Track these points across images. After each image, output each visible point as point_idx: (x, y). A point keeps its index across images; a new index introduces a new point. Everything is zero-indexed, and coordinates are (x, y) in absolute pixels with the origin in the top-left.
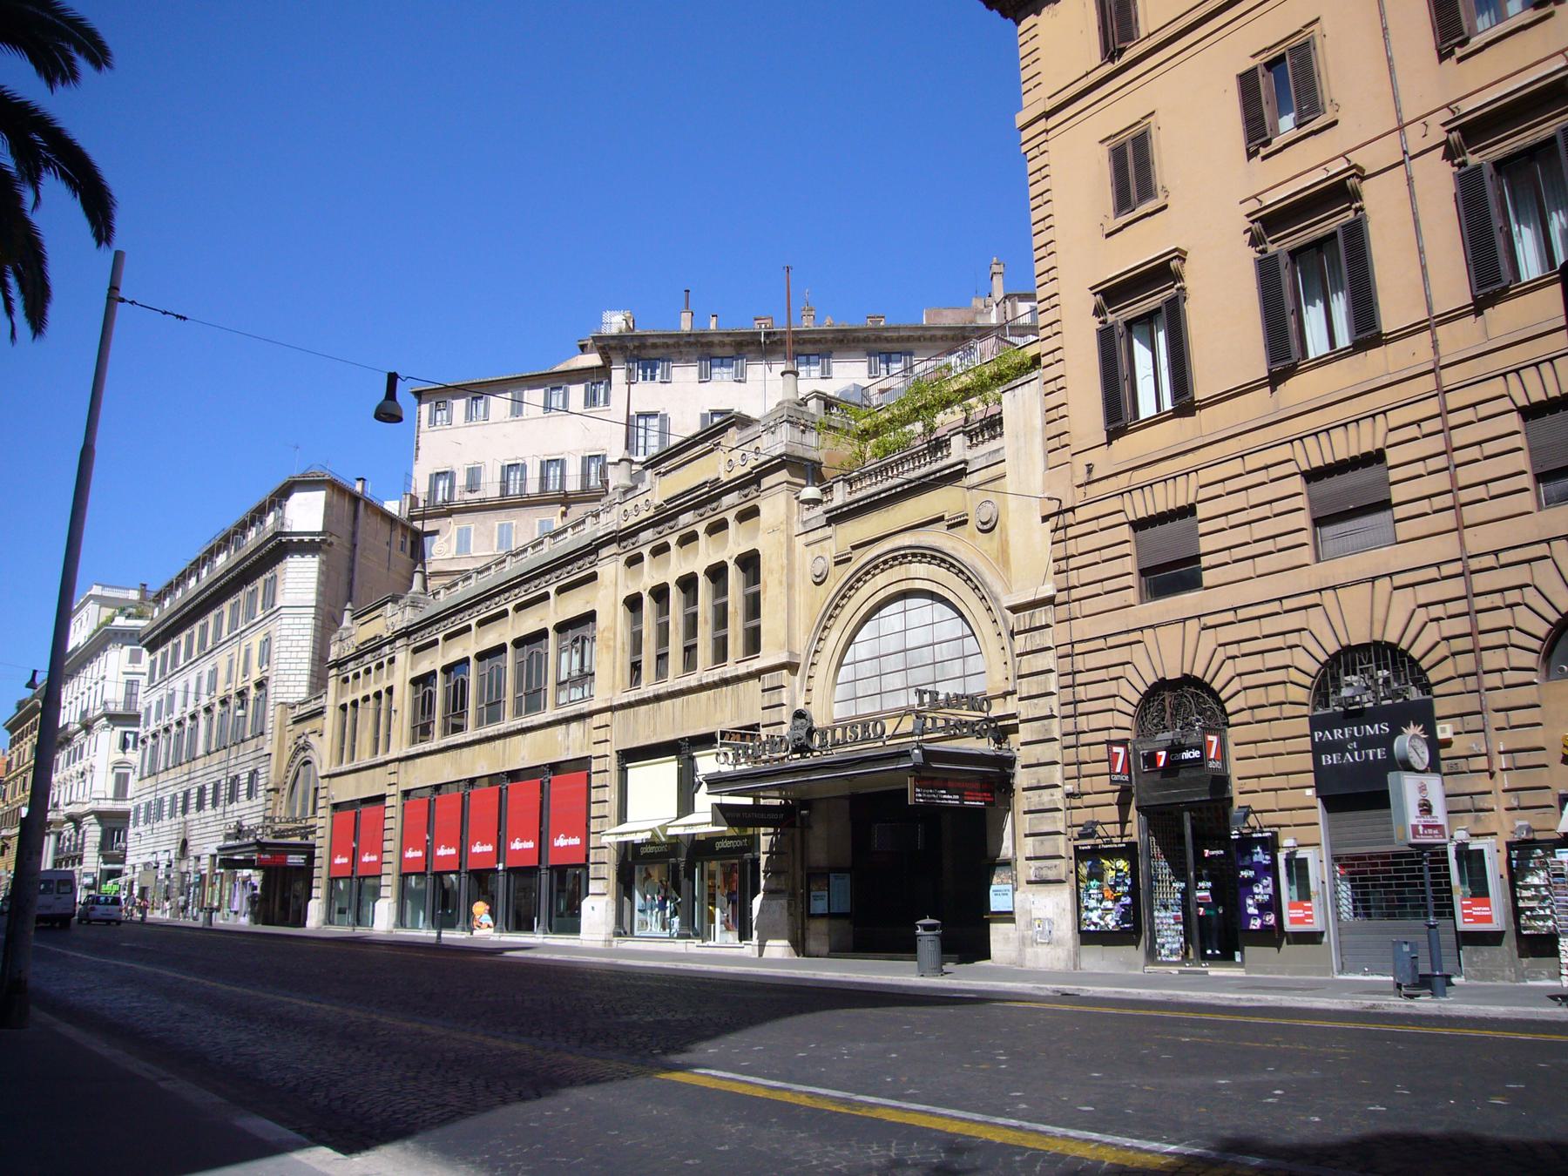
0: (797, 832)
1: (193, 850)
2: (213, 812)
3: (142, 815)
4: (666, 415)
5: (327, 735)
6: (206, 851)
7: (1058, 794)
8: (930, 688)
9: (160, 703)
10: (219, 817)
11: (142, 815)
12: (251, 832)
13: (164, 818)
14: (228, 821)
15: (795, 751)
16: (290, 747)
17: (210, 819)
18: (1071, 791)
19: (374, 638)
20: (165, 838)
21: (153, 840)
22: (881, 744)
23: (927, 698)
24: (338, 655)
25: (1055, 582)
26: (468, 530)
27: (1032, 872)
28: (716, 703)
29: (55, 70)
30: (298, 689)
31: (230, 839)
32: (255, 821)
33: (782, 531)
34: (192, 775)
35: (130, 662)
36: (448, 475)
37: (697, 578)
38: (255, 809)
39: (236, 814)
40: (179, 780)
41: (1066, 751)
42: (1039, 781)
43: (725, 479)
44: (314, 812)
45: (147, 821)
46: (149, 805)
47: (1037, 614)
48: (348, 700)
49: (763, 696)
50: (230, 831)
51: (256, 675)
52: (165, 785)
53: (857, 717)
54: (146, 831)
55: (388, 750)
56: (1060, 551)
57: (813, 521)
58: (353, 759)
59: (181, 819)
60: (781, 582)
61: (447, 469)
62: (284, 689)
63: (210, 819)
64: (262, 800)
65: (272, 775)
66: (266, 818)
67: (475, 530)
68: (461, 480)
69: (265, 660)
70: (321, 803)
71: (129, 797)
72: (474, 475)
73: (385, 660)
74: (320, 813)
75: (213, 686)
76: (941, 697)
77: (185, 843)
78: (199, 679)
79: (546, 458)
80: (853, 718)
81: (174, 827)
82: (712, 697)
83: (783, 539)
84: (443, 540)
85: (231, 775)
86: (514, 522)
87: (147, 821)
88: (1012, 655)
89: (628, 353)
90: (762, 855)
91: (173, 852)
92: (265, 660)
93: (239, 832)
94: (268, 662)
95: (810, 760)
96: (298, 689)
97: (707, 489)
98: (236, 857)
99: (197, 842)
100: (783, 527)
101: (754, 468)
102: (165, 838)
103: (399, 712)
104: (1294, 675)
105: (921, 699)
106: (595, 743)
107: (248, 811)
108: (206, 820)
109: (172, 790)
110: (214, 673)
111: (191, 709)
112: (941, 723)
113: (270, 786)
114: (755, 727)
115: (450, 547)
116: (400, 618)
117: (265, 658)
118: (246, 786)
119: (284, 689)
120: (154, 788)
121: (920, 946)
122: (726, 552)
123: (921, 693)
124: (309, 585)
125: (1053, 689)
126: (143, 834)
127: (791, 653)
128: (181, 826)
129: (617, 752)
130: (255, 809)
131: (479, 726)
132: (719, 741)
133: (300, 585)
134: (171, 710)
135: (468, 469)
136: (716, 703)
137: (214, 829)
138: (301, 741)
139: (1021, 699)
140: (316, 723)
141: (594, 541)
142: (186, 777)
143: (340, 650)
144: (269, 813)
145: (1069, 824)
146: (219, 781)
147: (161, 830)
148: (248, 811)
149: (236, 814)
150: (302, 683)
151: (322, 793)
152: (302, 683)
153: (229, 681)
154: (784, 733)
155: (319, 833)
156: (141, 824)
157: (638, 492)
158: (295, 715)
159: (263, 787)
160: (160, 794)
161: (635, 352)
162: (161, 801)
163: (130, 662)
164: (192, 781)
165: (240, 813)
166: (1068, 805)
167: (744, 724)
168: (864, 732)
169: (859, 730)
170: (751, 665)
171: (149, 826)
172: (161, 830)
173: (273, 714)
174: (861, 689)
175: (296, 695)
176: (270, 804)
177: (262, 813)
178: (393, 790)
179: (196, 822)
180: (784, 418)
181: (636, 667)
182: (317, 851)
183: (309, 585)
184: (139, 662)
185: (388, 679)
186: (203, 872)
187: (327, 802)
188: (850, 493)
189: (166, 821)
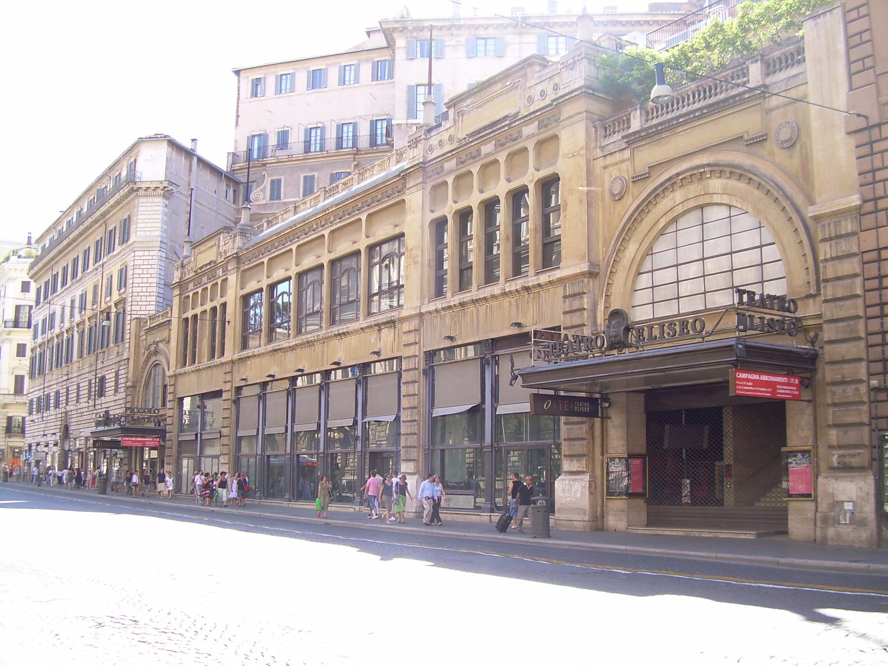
0: (597, 421)
1: (73, 433)
2: (87, 405)
3: (35, 406)
4: (440, 85)
5: (173, 343)
6: (82, 434)
7: (863, 388)
8: (748, 288)
9: (44, 321)
10: (91, 408)
11: (35, 406)
12: (117, 419)
13: (51, 408)
14: (98, 411)
15: (611, 347)
16: (144, 353)
17: (84, 410)
18: (877, 385)
19: (210, 263)
20: (52, 424)
21: (43, 426)
22: (701, 340)
23: (745, 298)
24: (180, 279)
25: (861, 194)
26: (279, 181)
27: (835, 459)
28: (518, 309)
29: (22, 377)
30: (148, 308)
31: (99, 426)
32: (118, 411)
33: (582, 156)
34: (70, 376)
35: (22, 292)
36: (263, 137)
37: (472, 211)
38: (118, 402)
39: (104, 406)
40: (60, 380)
41: (870, 349)
42: (843, 377)
43: (524, 113)
44: (164, 404)
45: (38, 411)
46: (39, 398)
47: (843, 223)
48: (189, 314)
49: (565, 302)
50: (100, 419)
51: (116, 297)
52: (50, 383)
53: (654, 319)
54: (38, 419)
55: (223, 355)
56: (867, 165)
57: (611, 146)
58: (194, 362)
59: (63, 410)
60: (581, 201)
61: (262, 132)
62: (138, 308)
63: (84, 410)
64: (123, 395)
65: (130, 375)
66: (127, 409)
67: (285, 182)
68: (273, 141)
69: (123, 284)
70: (169, 397)
71: (25, 393)
72: (283, 138)
73: (219, 281)
74: (169, 405)
75: (83, 308)
76: (757, 297)
77: (66, 429)
78: (73, 301)
79: (341, 123)
80: (650, 320)
81: (58, 416)
82: (514, 303)
83: (583, 162)
84: (258, 189)
85: (99, 375)
86: (316, 174)
87: (38, 411)
88: (440, 336)
89: (409, 35)
90: (563, 442)
91: (58, 434)
92: (123, 284)
93: (107, 420)
94: (125, 286)
95: (627, 354)
96: (148, 308)
97: (508, 122)
98: (106, 439)
99: (76, 427)
100: (583, 152)
101: (553, 101)
102: (52, 424)
103: (232, 323)
105: (741, 298)
106: (405, 345)
107: (112, 404)
108: (82, 411)
109: (55, 388)
110: (83, 297)
111: (67, 325)
112: (757, 321)
113: (129, 384)
114: (558, 328)
115: (264, 194)
116: (231, 246)
117: (123, 282)
118: (86, 391)
119: (138, 308)
120: (42, 386)
121: (11, 415)
122: (526, 177)
123: (741, 292)
124: (157, 217)
125: (859, 291)
126: (36, 421)
127: (592, 264)
128: (63, 415)
129: (425, 352)
130: (118, 402)
131: (244, 349)
132: (533, 339)
133: (149, 225)
134: (52, 327)
135: (279, 133)
136: (518, 309)
137: (88, 417)
138: (152, 348)
139: (826, 301)
140: (164, 334)
141: (402, 172)
142: (65, 378)
143: (182, 274)
144: (128, 405)
145: (873, 415)
146: (91, 380)
147: (49, 418)
148: (112, 404)
149: (104, 406)
150: (151, 303)
151: (170, 389)
152: (151, 303)
153: (94, 302)
154: (586, 334)
155: (169, 421)
156: (34, 413)
157: (442, 129)
158: (147, 327)
159: (124, 385)
160: (47, 391)
161: (415, 34)
162: (48, 395)
163: (22, 292)
164: (70, 381)
165: (107, 405)
166: (872, 399)
167: (549, 327)
168: (682, 330)
169: (678, 328)
170: (553, 275)
171: (40, 415)
172: (49, 418)
173: (130, 327)
174: (660, 294)
175: (147, 313)
176: (129, 398)
177: (123, 405)
178: (412, 351)
179: (73, 412)
180: (583, 55)
181: (440, 281)
182: (168, 435)
183: (157, 217)
184: (28, 291)
185: (221, 297)
186: (81, 450)
187: (175, 396)
188: (647, 121)
189: (52, 411)
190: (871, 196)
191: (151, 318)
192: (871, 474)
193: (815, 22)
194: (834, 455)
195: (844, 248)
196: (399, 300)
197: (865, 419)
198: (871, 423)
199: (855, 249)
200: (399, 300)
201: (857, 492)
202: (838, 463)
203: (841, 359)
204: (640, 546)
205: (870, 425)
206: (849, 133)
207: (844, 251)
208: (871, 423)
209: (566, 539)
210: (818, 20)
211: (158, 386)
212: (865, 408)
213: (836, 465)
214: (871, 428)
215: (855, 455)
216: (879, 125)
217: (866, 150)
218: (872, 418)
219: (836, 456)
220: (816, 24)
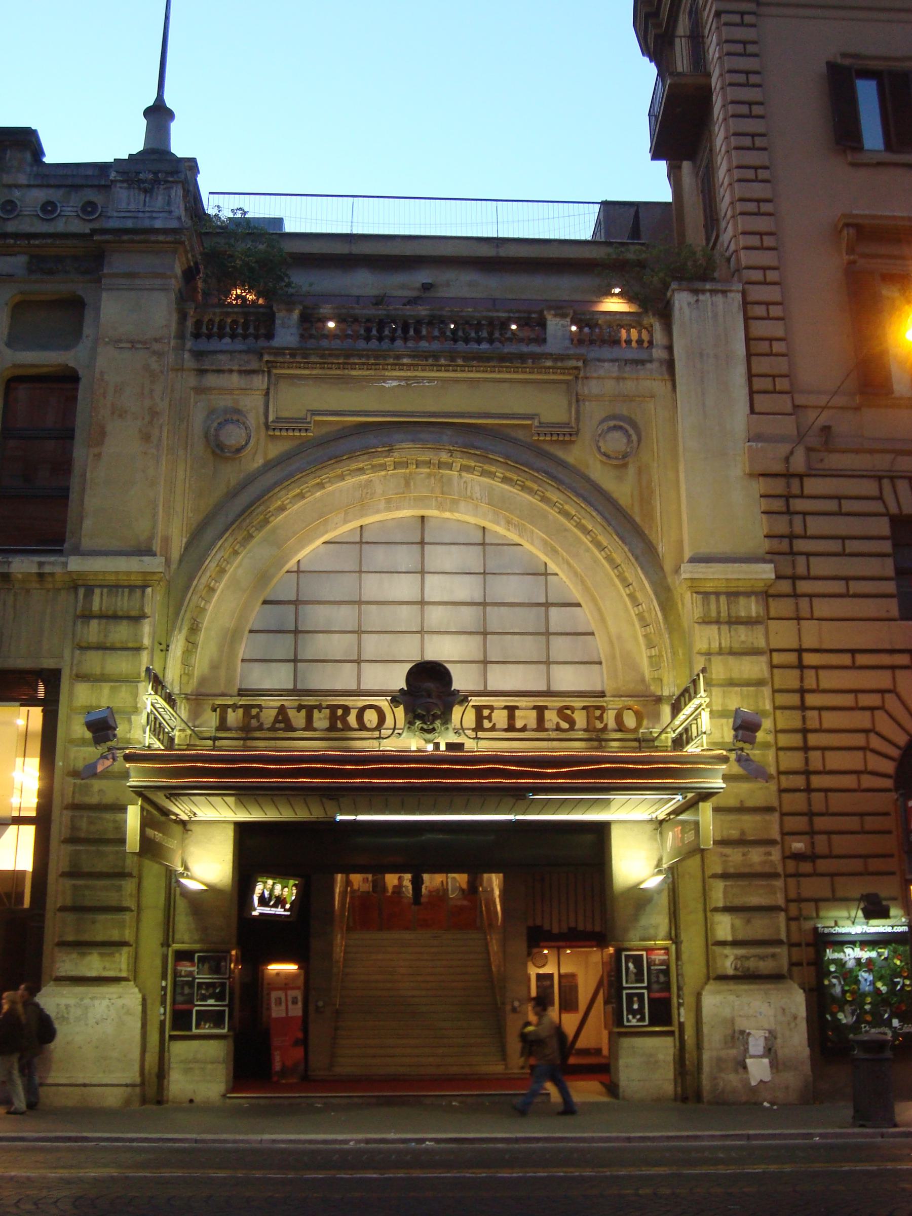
56: (781, 526)
104: (876, 742)
190: (789, 571)
191: (80, 662)
192: (796, 986)
193: (695, 298)
194: (727, 956)
195: (743, 638)
196: (36, 589)
197: (780, 900)
198: (787, 906)
199: (761, 643)
200: (36, 589)
201: (775, 1016)
202: (736, 969)
203: (738, 805)
204: (319, 1133)
205: (786, 910)
206: (751, 475)
207: (743, 642)
208: (787, 906)
209: (144, 1147)
210: (701, 297)
211: (175, 239)
212: (779, 883)
213: (730, 972)
214: (787, 915)
215: (767, 957)
216: (801, 477)
217: (778, 505)
218: (788, 901)
219: (731, 958)
220: (697, 301)
